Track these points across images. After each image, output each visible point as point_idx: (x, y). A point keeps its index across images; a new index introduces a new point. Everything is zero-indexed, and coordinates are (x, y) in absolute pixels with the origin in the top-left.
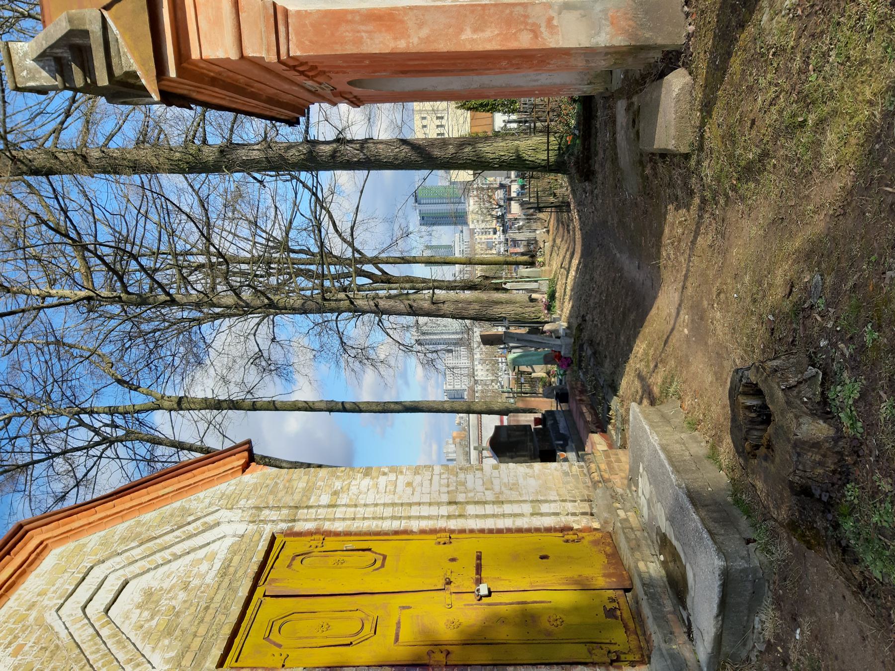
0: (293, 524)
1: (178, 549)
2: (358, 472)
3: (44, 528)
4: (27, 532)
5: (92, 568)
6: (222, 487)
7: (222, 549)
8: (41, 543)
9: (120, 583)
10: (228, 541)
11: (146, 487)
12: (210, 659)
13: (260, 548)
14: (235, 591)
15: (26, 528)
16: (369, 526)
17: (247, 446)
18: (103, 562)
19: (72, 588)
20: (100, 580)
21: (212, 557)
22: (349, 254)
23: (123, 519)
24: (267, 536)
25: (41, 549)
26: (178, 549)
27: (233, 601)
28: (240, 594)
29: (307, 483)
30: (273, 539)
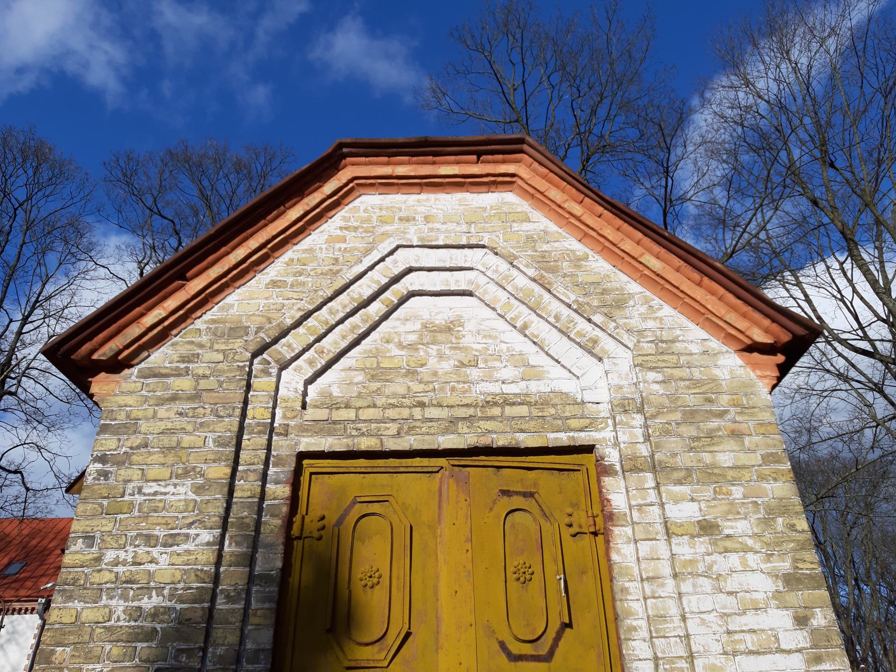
0: (620, 472)
1: (538, 327)
2: (795, 560)
3: (536, 165)
4: (522, 151)
5: (483, 247)
6: (694, 336)
7: (557, 381)
8: (513, 175)
9: (463, 287)
10: (569, 386)
11: (646, 235)
12: (311, 440)
13: (552, 436)
14: (446, 431)
15: (525, 147)
16: (629, 613)
17: (800, 331)
18: (496, 254)
19: (441, 242)
20: (464, 265)
21: (531, 372)
22: (30, 320)
23: (584, 237)
24: (583, 438)
25: (504, 182)
26: (538, 327)
27: (428, 434)
28: (441, 439)
29: (734, 468)
30: (589, 449)
